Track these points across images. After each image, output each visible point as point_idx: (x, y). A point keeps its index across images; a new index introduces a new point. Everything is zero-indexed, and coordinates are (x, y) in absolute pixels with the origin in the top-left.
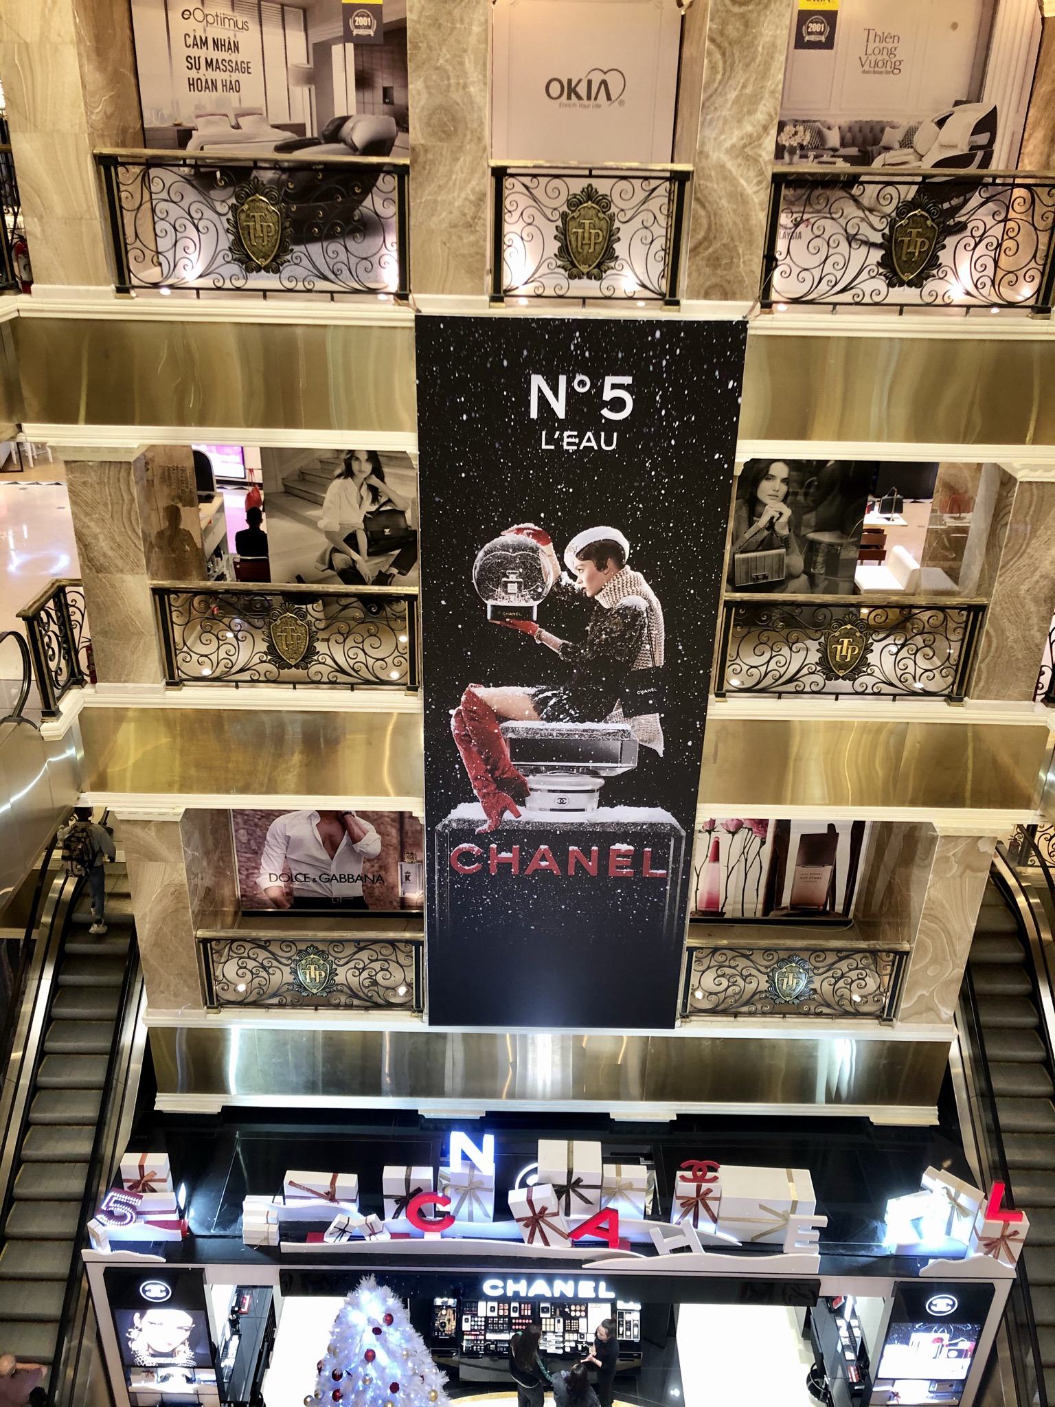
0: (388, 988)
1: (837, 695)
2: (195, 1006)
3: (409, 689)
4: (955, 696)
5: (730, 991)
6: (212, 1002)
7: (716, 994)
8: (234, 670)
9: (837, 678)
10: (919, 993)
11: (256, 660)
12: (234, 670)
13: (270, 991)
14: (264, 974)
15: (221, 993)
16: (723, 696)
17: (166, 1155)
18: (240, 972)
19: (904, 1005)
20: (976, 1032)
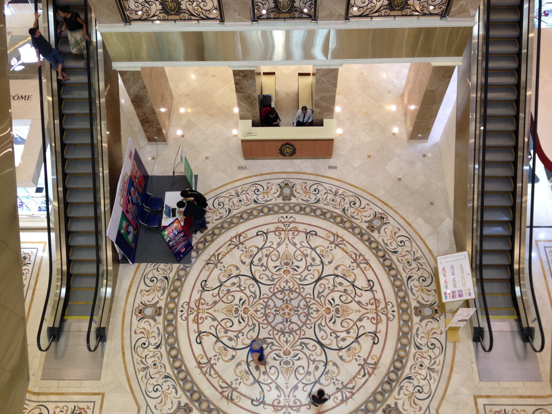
0: (206, 11)
1: (395, 16)
2: (119, 22)
3: (220, 21)
4: (444, 15)
5: (369, 6)
6: (126, 20)
7: (362, 7)
8: (150, 16)
9: (395, 10)
10: (461, 3)
11: (158, 12)
12: (150, 16)
13: (152, 14)
14: (147, 5)
15: (129, 15)
16: (348, 19)
17: (166, 193)
18: (136, 4)
19: (453, 9)
20: (488, 25)
